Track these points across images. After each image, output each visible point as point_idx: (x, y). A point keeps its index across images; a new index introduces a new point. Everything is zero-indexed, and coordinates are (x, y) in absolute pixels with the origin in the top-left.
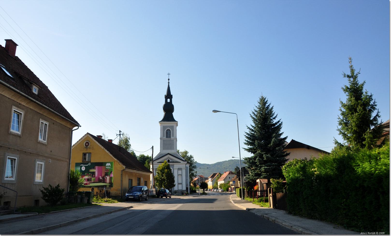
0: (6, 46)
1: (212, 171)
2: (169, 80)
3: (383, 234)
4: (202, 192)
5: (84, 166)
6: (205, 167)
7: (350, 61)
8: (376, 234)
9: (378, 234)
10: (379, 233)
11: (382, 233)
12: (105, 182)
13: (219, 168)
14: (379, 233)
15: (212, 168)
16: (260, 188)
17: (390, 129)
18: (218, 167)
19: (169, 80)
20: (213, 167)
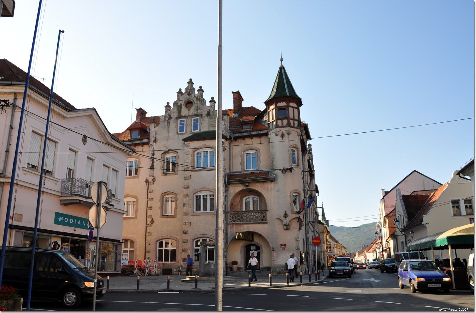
0: (149, 118)
1: (357, 237)
2: (282, 60)
3: (466, 311)
4: (392, 240)
5: (112, 243)
6: (344, 231)
7: (366, 257)
8: (458, 311)
9: (461, 311)
10: (461, 309)
11: (465, 310)
12: (272, 280)
13: (367, 233)
14: (461, 309)
15: (356, 232)
16: (109, 300)
17: (474, 217)
18: (364, 232)
19: (282, 60)
20: (358, 232)
